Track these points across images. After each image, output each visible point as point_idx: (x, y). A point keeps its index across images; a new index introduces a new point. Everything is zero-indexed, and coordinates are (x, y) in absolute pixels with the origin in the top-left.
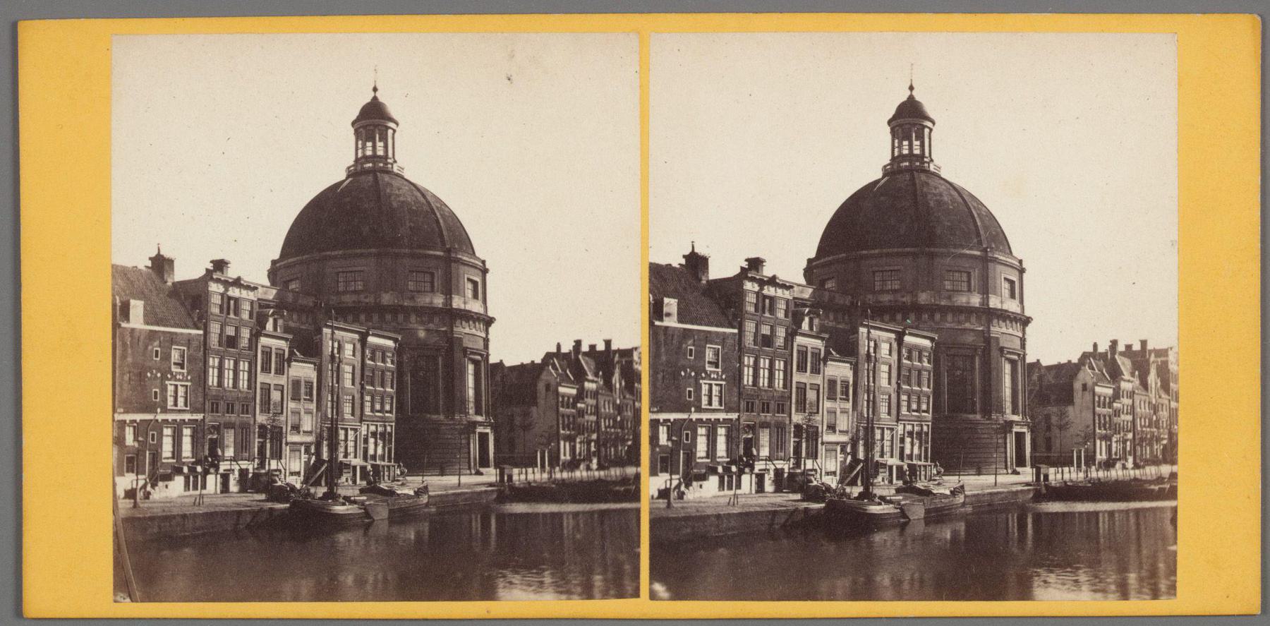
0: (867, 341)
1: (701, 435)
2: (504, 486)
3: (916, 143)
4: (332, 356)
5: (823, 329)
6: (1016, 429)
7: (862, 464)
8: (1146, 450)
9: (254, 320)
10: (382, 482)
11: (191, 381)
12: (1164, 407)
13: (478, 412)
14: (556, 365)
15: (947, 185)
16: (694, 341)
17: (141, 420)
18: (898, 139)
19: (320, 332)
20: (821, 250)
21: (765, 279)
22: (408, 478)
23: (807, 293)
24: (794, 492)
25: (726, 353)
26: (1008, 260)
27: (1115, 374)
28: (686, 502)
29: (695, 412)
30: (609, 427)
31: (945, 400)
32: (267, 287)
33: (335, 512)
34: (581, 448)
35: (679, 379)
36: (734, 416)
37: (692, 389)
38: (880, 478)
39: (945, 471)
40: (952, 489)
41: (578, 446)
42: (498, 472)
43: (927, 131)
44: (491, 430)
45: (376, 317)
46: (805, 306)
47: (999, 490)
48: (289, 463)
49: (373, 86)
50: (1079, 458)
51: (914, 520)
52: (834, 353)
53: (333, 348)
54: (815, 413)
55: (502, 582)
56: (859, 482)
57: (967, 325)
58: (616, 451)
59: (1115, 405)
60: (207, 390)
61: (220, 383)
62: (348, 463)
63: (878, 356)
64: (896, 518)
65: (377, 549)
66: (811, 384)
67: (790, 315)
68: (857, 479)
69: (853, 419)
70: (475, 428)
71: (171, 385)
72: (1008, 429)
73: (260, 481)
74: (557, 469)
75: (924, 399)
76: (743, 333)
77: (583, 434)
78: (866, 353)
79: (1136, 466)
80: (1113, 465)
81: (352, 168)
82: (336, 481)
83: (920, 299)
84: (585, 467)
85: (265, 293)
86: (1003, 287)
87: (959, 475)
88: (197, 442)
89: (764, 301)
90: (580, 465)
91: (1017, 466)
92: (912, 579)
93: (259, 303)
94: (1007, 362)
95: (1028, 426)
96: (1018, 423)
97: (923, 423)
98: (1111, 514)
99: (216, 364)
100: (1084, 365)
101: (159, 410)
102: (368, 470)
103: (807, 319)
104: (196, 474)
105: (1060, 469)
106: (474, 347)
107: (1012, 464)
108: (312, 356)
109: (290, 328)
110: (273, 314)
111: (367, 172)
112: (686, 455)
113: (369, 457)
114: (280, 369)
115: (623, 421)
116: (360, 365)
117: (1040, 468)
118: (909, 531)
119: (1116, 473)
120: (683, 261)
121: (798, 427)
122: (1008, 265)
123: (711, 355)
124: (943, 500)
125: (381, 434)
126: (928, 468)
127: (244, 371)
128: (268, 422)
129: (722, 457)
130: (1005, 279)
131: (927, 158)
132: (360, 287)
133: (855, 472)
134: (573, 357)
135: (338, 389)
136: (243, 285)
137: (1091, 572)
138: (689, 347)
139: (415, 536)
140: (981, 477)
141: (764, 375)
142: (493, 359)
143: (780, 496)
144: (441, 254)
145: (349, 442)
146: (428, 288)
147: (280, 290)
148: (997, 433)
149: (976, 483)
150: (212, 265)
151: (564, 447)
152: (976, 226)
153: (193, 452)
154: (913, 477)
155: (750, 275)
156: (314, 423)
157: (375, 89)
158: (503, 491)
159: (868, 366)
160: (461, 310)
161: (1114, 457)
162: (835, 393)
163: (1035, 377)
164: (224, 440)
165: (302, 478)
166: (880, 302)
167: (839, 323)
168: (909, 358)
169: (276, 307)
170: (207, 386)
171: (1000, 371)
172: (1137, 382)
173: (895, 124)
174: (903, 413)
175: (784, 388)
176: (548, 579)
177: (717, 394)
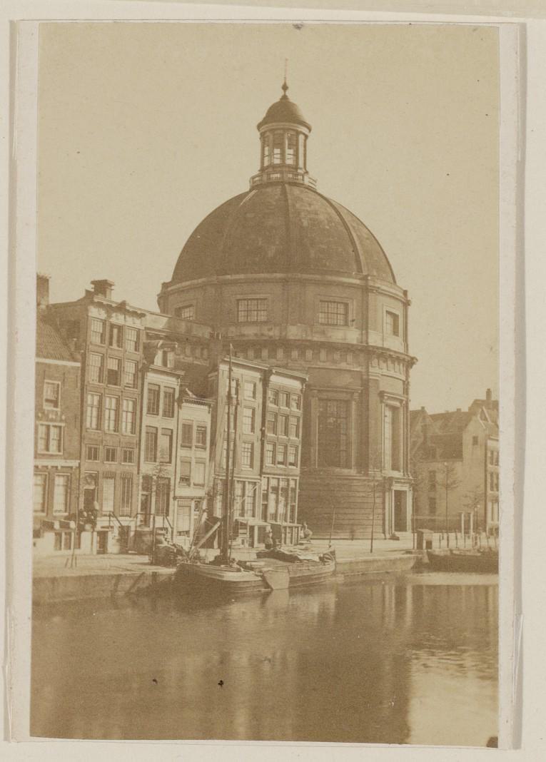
2: (422, 553)
6: (396, 487)
7: (219, 524)
9: (140, 353)
10: (284, 545)
11: (65, 421)
19: (215, 368)
21: (114, 305)
23: (161, 323)
24: (141, 553)
26: (391, 290)
39: (313, 534)
40: (322, 556)
45: (280, 353)
46: (158, 337)
48: (177, 520)
49: (283, 83)
50: (468, 522)
53: (230, 387)
57: (343, 365)
61: (99, 426)
62: (245, 522)
67: (141, 348)
71: (42, 425)
72: (387, 487)
73: (143, 542)
78: (227, 394)
81: (257, 179)
82: (230, 543)
86: (385, 321)
89: (111, 331)
91: (396, 530)
94: (387, 408)
99: (96, 403)
100: (475, 414)
102: (267, 531)
103: (160, 354)
105: (445, 536)
116: (261, 408)
118: (271, 602)
128: (154, 473)
131: (301, 169)
136: (128, 311)
137: (478, 655)
140: (354, 542)
141: (109, 418)
144: (358, 282)
150: (93, 286)
152: (355, 250)
154: (277, 540)
155: (96, 300)
157: (285, 88)
158: (421, 559)
159: (229, 409)
163: (418, 427)
166: (244, 335)
168: (276, 402)
173: (266, 129)
177: (55, 437)
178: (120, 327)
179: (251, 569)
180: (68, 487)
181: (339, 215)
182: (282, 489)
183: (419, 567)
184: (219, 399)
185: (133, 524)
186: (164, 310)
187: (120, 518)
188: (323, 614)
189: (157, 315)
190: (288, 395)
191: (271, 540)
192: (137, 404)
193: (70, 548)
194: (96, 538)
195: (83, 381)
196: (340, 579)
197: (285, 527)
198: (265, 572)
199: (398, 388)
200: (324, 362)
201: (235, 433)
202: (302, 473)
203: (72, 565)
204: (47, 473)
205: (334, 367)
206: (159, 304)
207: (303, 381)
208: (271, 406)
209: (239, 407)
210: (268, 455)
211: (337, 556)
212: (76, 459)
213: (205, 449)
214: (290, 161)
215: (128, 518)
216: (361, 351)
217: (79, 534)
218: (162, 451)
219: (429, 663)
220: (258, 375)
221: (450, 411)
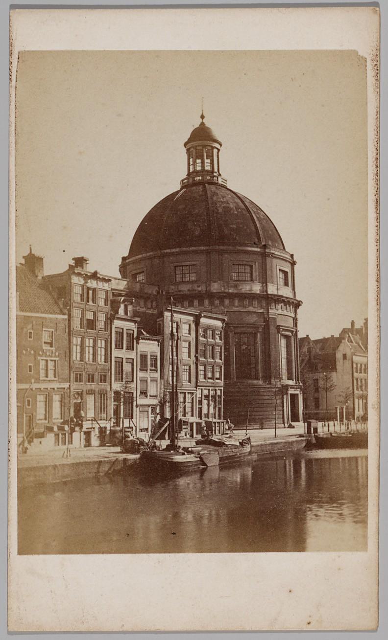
0: (171, 323)
3: (207, 161)
5: (136, 314)
6: (291, 391)
7: (168, 422)
9: (109, 307)
10: (214, 435)
18: (192, 158)
21: (89, 274)
23: (122, 285)
25: (59, 335)
26: (282, 254)
33: (176, 461)
38: (183, 433)
40: (241, 441)
43: (215, 151)
46: (120, 295)
47: (278, 441)
49: (201, 114)
50: (341, 414)
51: (210, 466)
52: (145, 333)
57: (251, 309)
61: (82, 359)
63: (179, 335)
64: (196, 465)
66: (127, 358)
67: (109, 302)
68: (165, 433)
69: (161, 386)
75: (217, 369)
82: (176, 435)
83: (212, 289)
85: (118, 284)
87: (246, 429)
88: (64, 407)
91: (292, 421)
92: (210, 515)
93: (113, 293)
96: (292, 387)
97: (217, 388)
99: (79, 343)
100: (344, 339)
102: (202, 426)
103: (122, 306)
104: (65, 432)
105: (326, 423)
106: (286, 325)
112: (28, 417)
117: (310, 422)
118: (207, 475)
121: (117, 393)
124: (233, 450)
126: (222, 425)
128: (122, 389)
130: (280, 270)
131: (216, 173)
132: (193, 278)
133: (163, 428)
135: (177, 361)
136: (99, 278)
137: (353, 506)
139: (241, 479)
143: (104, 449)
149: (260, 436)
155: (76, 271)
157: (202, 117)
162: (146, 365)
169: (126, 295)
171: (277, 347)
173: (191, 146)
174: (201, 380)
177: (52, 368)
183: (309, 446)
184: (165, 337)
185: (108, 425)
187: (99, 422)
190: (213, 331)
192: (108, 342)
193: (65, 444)
194: (83, 437)
197: (215, 423)
201: (177, 359)
203: (67, 456)
204: (47, 393)
205: (245, 310)
208: (201, 339)
209: (179, 341)
212: (67, 382)
213: (157, 371)
214: (208, 168)
217: (71, 434)
218: (127, 374)
219: (319, 513)
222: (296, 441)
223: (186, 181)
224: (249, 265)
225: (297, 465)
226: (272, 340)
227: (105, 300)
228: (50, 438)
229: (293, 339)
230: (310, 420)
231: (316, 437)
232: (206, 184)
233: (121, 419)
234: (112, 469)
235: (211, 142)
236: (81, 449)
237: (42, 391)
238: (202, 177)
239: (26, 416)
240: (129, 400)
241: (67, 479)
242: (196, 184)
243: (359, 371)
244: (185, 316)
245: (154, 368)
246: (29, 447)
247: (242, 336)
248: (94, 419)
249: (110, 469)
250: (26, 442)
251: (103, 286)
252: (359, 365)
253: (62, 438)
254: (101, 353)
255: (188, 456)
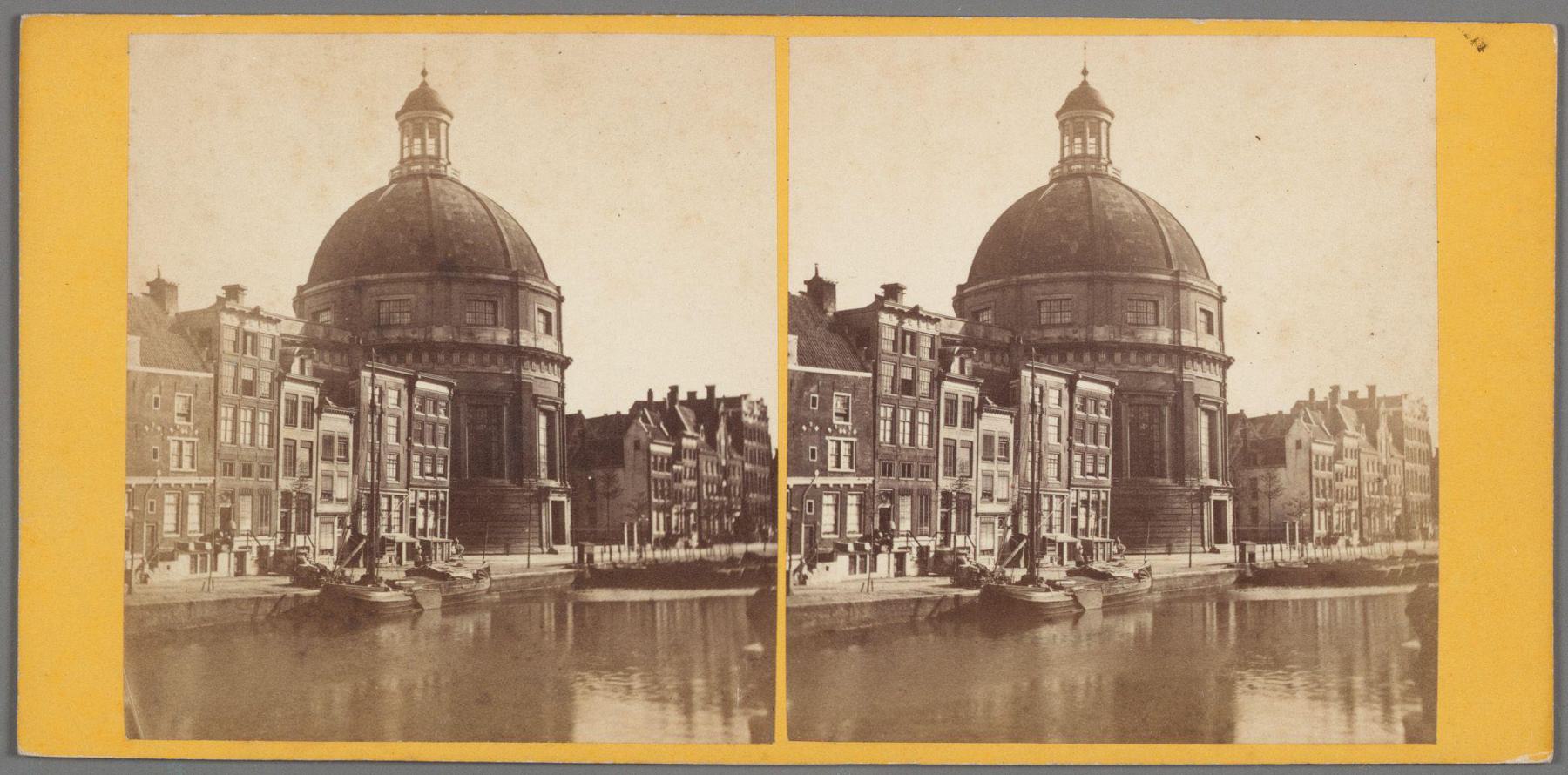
0: (370, 388)
1: (828, 505)
2: (584, 568)
3: (1091, 141)
4: (373, 406)
5: (976, 372)
6: (1215, 497)
7: (1025, 541)
8: (1375, 523)
9: (936, 360)
12: (1397, 469)
13: (551, 475)
14: (647, 417)
15: (1129, 192)
16: (161, 388)
17: (795, 486)
18: (408, 136)
20: (974, 275)
21: (906, 310)
22: (465, 557)
23: (957, 328)
27: (1336, 428)
28: (808, 589)
29: (163, 475)
30: (712, 494)
31: (1127, 461)
32: (952, 319)
33: (375, 600)
34: (678, 521)
35: (799, 435)
36: (868, 481)
37: (815, 448)
40: (475, 572)
41: (674, 518)
42: (576, 551)
44: (568, 497)
45: (1087, 357)
46: (294, 344)
53: (1033, 394)
54: (967, 477)
55: (581, 687)
56: (361, 563)
57: (1155, 368)
58: (721, 524)
59: (675, 467)
60: (877, 448)
61: (893, 440)
62: (392, 538)
63: (1044, 406)
65: (1089, 645)
67: (937, 354)
70: (548, 495)
71: (832, 441)
72: (1205, 497)
74: (649, 546)
75: (1101, 460)
76: (879, 378)
77: (681, 503)
78: (1030, 402)
79: (1363, 542)
80: (1335, 541)
81: (1057, 170)
82: (1037, 561)
83: (435, 337)
84: (683, 544)
90: (676, 541)
91: (1216, 543)
94: (1203, 413)
95: (1230, 492)
97: (1101, 490)
98: (1332, 602)
99: (889, 415)
100: (1298, 416)
101: (817, 473)
103: (957, 360)
107: (1210, 540)
108: (347, 405)
109: (321, 370)
110: (960, 353)
111: (1077, 175)
113: (417, 531)
114: (308, 421)
115: (730, 486)
116: (406, 416)
118: (1083, 622)
119: (1339, 552)
120: (805, 289)
121: (946, 494)
122: (543, 293)
123: (839, 405)
124: (1125, 586)
125: (432, 502)
126: (1107, 546)
127: (263, 424)
129: (853, 532)
130: (1201, 310)
131: (443, 159)
133: (1017, 550)
134: (1329, 407)
136: (262, 317)
138: (812, 395)
139: (474, 630)
140: (1172, 556)
141: (904, 430)
142: (570, 410)
145: (392, 513)
146: (1152, 321)
147: (307, 323)
148: (1192, 502)
149: (507, 564)
150: (883, 290)
151: (658, 519)
153: (860, 525)
155: (886, 306)
156: (350, 489)
157: (1085, 72)
160: (529, 348)
161: (674, 532)
163: (1238, 432)
164: (898, 510)
165: (335, 557)
167: (336, 365)
168: (1083, 409)
169: (964, 344)
170: (877, 444)
172: (1363, 437)
174: (1076, 477)
175: (929, 446)
176: (637, 683)
177: (847, 454)
178: (255, 334)
179: (1061, 588)
180: (203, 506)
181: (1148, 208)
182: (1093, 502)
183: (1243, 581)
184: (1023, 408)
185: (272, 543)
186: (300, 315)
187: (259, 538)
188: (1140, 635)
189: (952, 319)
190: (435, 402)
191: (1082, 557)
192: (275, 415)
193: (206, 571)
194: (893, 560)
195: (875, 391)
196: (1157, 597)
197: (1097, 543)
198: (416, 591)
199: (1215, 391)
200: (1133, 365)
201: (1040, 443)
202: (1114, 483)
203: (868, 590)
204: (839, 492)
205: (1146, 370)
206: (294, 307)
207: (1111, 386)
208: (1078, 413)
209: (1043, 415)
210: (1077, 466)
211: (492, 572)
212: (210, 476)
213: (1008, 461)
214: (1092, 151)
215: (927, 538)
216: (1173, 351)
217: (215, 556)
218: (302, 464)
219: (596, 685)
220: (1063, 381)
221: (1271, 414)
222: (561, 574)
223: (397, 171)
224: (492, 302)
225: (1222, 607)
226: (1187, 417)
227: (931, 349)
228: (184, 560)
229: (557, 415)
230: (1244, 542)
231: (1253, 568)
232: (1089, 177)
233: (953, 535)
234: (937, 611)
235: (1097, 112)
236: (229, 579)
237: (173, 489)
238: (422, 165)
239: (147, 527)
240: (305, 504)
241: (868, 626)
242: (413, 176)
243: (1320, 468)
244: (393, 378)
245: (1003, 457)
246: (809, 575)
247: (478, 410)
248: (251, 534)
249: (933, 611)
250: (147, 566)
251: (269, 330)
252: (1321, 458)
253: (201, 561)
254: (263, 431)
255: (393, 593)
